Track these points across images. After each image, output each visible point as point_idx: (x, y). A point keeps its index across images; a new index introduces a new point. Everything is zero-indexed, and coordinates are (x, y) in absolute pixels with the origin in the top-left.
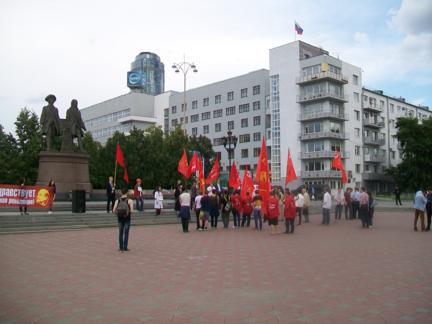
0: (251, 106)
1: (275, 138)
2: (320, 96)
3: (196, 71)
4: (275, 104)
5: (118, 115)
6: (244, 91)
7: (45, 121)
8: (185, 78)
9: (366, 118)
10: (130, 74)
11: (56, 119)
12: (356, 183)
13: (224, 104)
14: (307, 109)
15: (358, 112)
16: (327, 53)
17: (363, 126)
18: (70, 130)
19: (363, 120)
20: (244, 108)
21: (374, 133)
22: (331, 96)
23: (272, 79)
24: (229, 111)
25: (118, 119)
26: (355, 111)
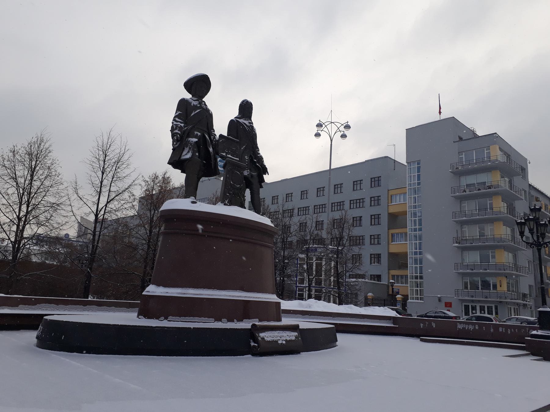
0: (367, 201)
14: (466, 206)
24: (317, 208)
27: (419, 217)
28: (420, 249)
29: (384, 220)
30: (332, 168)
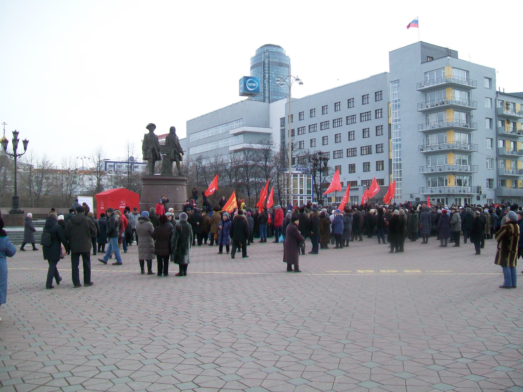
2: (443, 104)
3: (301, 83)
5: (230, 125)
6: (364, 98)
9: (502, 125)
10: (247, 79)
12: (487, 199)
19: (497, 128)
20: (365, 116)
21: (512, 143)
22: (454, 104)
24: (363, 116)
27: (399, 129)
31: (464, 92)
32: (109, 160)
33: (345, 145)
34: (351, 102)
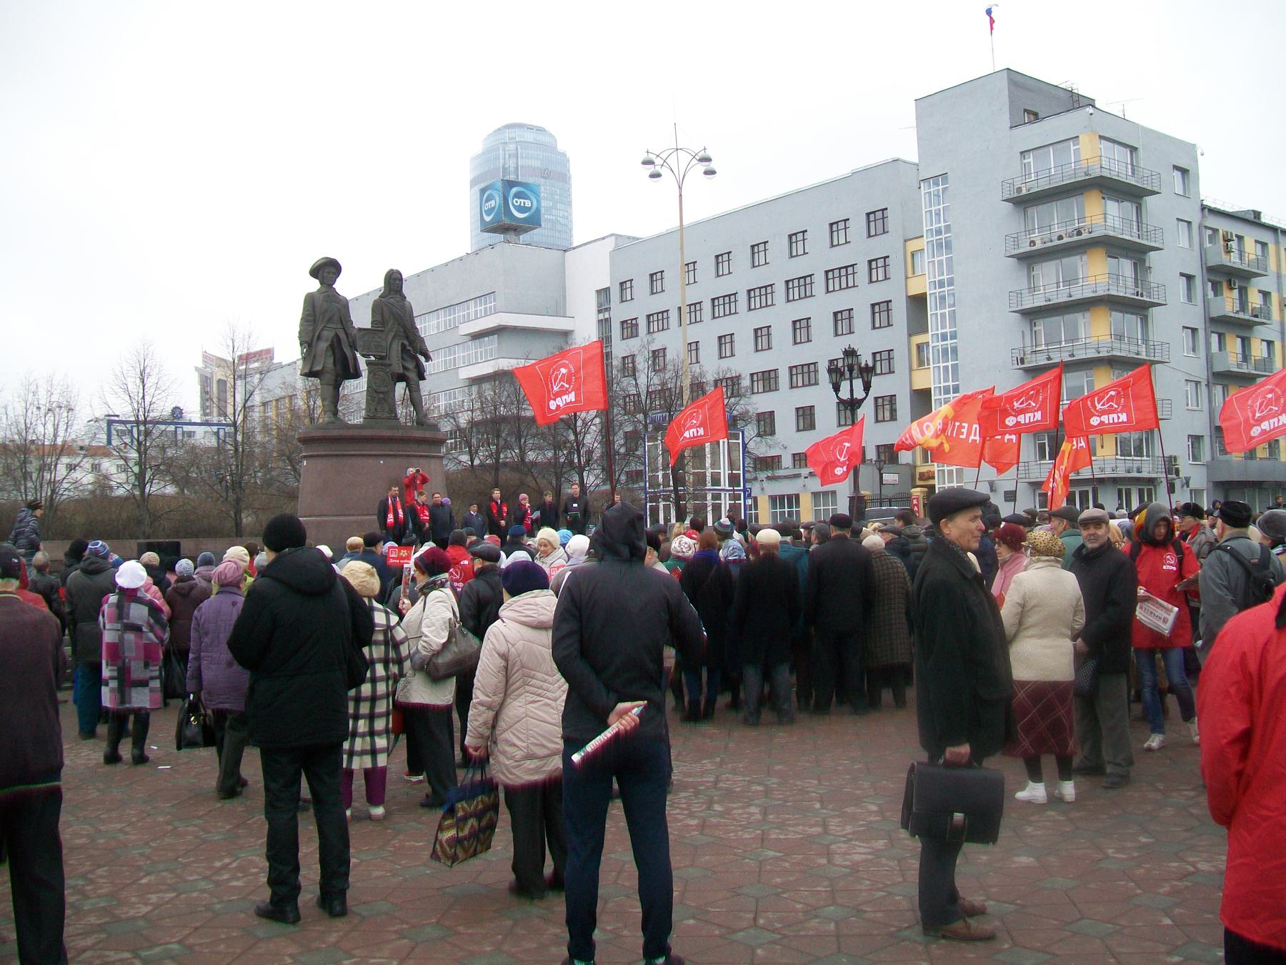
1: (941, 365)
2: (1079, 233)
3: (710, 172)
4: (940, 263)
5: (460, 313)
7: (313, 336)
8: (680, 195)
9: (1216, 295)
11: (344, 329)
12: (1191, 491)
13: (779, 269)
15: (1189, 278)
16: (1091, 103)
17: (1207, 319)
18: (387, 362)
19: (1206, 302)
20: (724, 304)
22: (1111, 233)
23: (926, 187)
24: (833, 278)
25: (460, 326)
26: (1182, 275)
28: (950, 270)
29: (900, 312)
30: (686, 223)
31: (1127, 205)
32: (118, 416)
33: (783, 356)
34: (758, 252)
